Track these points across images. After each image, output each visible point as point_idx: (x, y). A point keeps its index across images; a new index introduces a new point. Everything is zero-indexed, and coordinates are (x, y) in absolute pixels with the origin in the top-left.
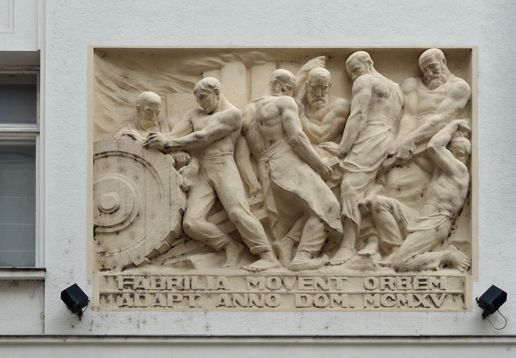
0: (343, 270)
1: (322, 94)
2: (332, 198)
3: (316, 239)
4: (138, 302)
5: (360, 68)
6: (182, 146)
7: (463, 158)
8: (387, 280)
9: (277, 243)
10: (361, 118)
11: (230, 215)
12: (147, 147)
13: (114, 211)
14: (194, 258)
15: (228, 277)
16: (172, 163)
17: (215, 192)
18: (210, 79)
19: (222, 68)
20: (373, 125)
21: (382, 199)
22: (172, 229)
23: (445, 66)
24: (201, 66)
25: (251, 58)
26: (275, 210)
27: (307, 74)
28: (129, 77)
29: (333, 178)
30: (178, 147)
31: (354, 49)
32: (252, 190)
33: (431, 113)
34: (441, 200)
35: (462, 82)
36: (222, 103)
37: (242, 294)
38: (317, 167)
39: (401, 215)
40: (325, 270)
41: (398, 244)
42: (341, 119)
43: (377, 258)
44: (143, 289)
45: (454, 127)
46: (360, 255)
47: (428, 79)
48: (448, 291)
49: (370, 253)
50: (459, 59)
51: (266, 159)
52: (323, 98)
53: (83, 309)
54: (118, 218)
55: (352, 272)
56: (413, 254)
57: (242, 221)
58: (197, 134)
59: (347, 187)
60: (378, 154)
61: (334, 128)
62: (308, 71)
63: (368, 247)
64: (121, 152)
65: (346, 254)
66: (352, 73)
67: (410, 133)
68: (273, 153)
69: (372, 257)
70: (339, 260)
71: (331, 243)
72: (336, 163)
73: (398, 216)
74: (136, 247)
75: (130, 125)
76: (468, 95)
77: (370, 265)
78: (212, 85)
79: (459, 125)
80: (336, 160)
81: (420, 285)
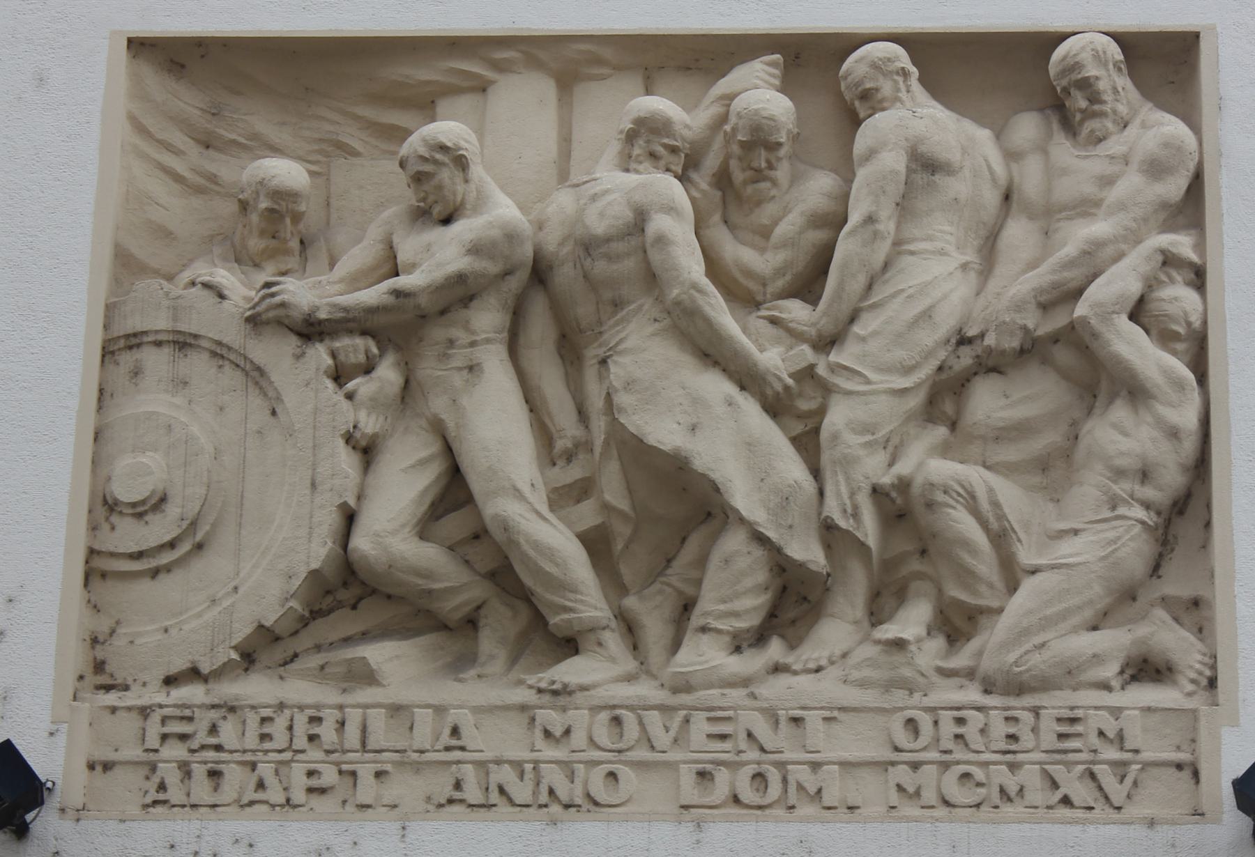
0: (828, 688)
1: (768, 162)
2: (793, 469)
3: (744, 593)
4: (201, 789)
5: (877, 90)
6: (353, 320)
7: (1180, 346)
8: (960, 721)
9: (631, 602)
10: (876, 235)
11: (488, 520)
12: (255, 322)
13: (145, 509)
14: (377, 653)
15: (477, 710)
16: (323, 367)
17: (448, 449)
18: (448, 128)
19: (490, 90)
20: (912, 253)
21: (943, 469)
22: (315, 565)
23: (1124, 82)
24: (428, 83)
25: (570, 62)
26: (623, 504)
27: (729, 105)
28: (227, 114)
29: (797, 409)
30: (348, 320)
31: (863, 34)
32: (560, 444)
33: (1086, 215)
34: (1119, 473)
35: (1173, 127)
36: (479, 192)
37: (518, 766)
38: (747, 378)
39: (1001, 517)
40: (776, 690)
41: (995, 604)
42: (817, 236)
43: (930, 653)
44: (218, 748)
45: (1148, 259)
46: (878, 642)
47: (1078, 117)
48: (1147, 755)
49: (904, 636)
50: (1167, 62)
51: (601, 352)
52: (772, 173)
53: (29, 817)
54: (158, 530)
55: (854, 696)
56: (1037, 640)
57: (522, 541)
58: (397, 286)
59: (835, 437)
60: (929, 337)
61: (801, 258)
62: (730, 98)
63: (902, 614)
64: (180, 332)
65: (836, 633)
66: (857, 103)
67: (1025, 272)
68: (622, 335)
69: (913, 648)
70: (815, 655)
71: (793, 603)
72: (804, 364)
73: (992, 519)
74: (209, 616)
75: (217, 250)
76: (1192, 166)
77: (907, 672)
78: (449, 144)
79: (1163, 252)
80: (805, 354)
81: (1062, 736)
